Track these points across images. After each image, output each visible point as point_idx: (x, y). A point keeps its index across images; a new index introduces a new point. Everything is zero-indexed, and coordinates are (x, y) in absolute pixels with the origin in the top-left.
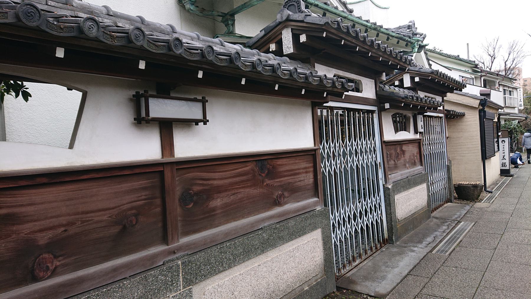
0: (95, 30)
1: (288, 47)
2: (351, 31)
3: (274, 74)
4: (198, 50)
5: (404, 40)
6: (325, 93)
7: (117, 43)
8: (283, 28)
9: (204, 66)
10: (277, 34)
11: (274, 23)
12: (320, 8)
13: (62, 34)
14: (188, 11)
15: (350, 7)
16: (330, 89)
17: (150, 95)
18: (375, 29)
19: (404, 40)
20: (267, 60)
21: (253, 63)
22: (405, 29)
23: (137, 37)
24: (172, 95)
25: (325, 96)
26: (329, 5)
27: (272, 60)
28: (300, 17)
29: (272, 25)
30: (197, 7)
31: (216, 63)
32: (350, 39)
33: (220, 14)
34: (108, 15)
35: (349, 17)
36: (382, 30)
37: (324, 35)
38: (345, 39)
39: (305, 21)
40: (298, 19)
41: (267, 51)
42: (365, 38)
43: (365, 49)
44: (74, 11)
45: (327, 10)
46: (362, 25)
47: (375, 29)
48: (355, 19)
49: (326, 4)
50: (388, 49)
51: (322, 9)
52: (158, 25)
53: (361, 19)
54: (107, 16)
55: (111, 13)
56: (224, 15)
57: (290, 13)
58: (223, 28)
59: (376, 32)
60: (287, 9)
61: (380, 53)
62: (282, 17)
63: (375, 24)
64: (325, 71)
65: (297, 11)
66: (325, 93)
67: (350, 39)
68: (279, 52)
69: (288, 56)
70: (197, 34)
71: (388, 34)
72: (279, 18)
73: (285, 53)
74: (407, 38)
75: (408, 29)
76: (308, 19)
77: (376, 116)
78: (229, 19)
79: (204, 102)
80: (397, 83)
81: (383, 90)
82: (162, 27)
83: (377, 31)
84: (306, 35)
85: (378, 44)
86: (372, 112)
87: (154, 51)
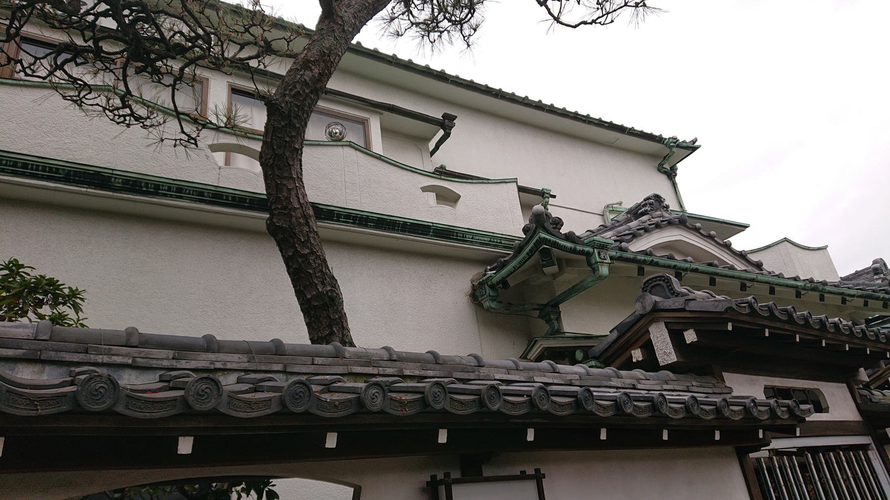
0: (379, 401)
1: (666, 352)
2: (777, 314)
3: (657, 413)
4: (522, 396)
5: (877, 299)
6: (761, 431)
7: (408, 412)
8: (650, 323)
9: (535, 420)
10: (640, 334)
11: (632, 318)
12: (703, 272)
13: (336, 415)
14: (489, 310)
15: (754, 258)
16: (768, 422)
17: (454, 480)
18: (814, 289)
19: (877, 299)
20: (635, 382)
21: (616, 401)
22: (869, 276)
23: (435, 395)
24: (487, 472)
25: (761, 436)
26: (717, 266)
27: (647, 384)
28: (676, 304)
29: (628, 320)
30: (501, 302)
31: (554, 412)
32: (778, 325)
33: (536, 307)
34: (391, 360)
35: (760, 278)
36: (827, 288)
37: (730, 328)
38: (769, 327)
39: (687, 309)
40: (673, 307)
41: (629, 365)
42: (806, 319)
43: (812, 335)
44: (347, 365)
45: (717, 274)
46: (787, 286)
47: (814, 289)
48: (771, 279)
49: (710, 265)
50: (857, 329)
51: (707, 273)
52: (457, 360)
53: (783, 278)
54: (389, 363)
55: (395, 357)
56: (542, 308)
57: (658, 299)
58: (543, 326)
59: (817, 294)
60: (650, 292)
61: (844, 338)
62: (644, 308)
63: (811, 281)
64: (747, 388)
65: (668, 293)
66: (761, 431)
67: (778, 325)
68: (651, 363)
69: (670, 367)
70: (513, 361)
71: (842, 294)
72: (638, 308)
73: (661, 364)
74: (882, 295)
75: (876, 274)
76: (692, 306)
77: (874, 455)
78: (550, 311)
79: (538, 478)
80: (637, 355)
81: (870, 400)
82: (464, 361)
83: (819, 291)
84: (695, 330)
85: (835, 323)
86: (865, 448)
87: (460, 413)
